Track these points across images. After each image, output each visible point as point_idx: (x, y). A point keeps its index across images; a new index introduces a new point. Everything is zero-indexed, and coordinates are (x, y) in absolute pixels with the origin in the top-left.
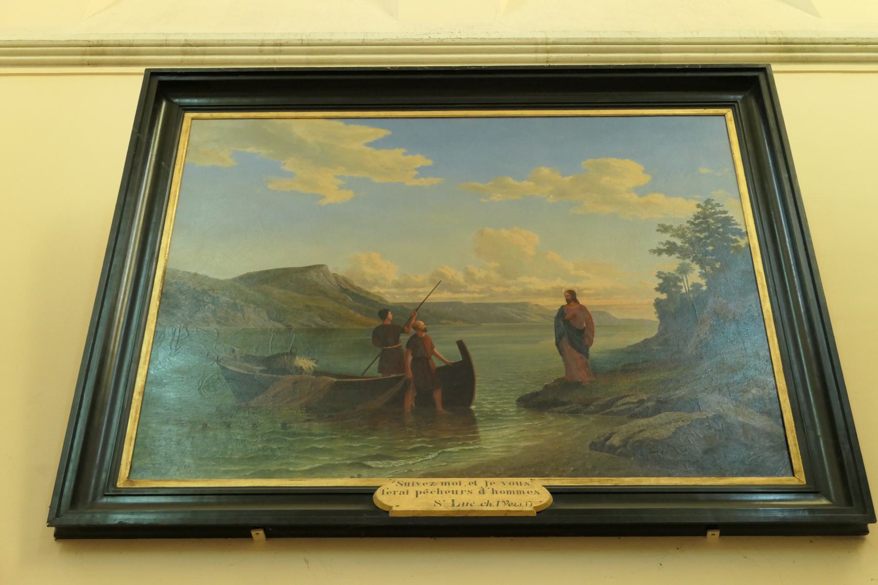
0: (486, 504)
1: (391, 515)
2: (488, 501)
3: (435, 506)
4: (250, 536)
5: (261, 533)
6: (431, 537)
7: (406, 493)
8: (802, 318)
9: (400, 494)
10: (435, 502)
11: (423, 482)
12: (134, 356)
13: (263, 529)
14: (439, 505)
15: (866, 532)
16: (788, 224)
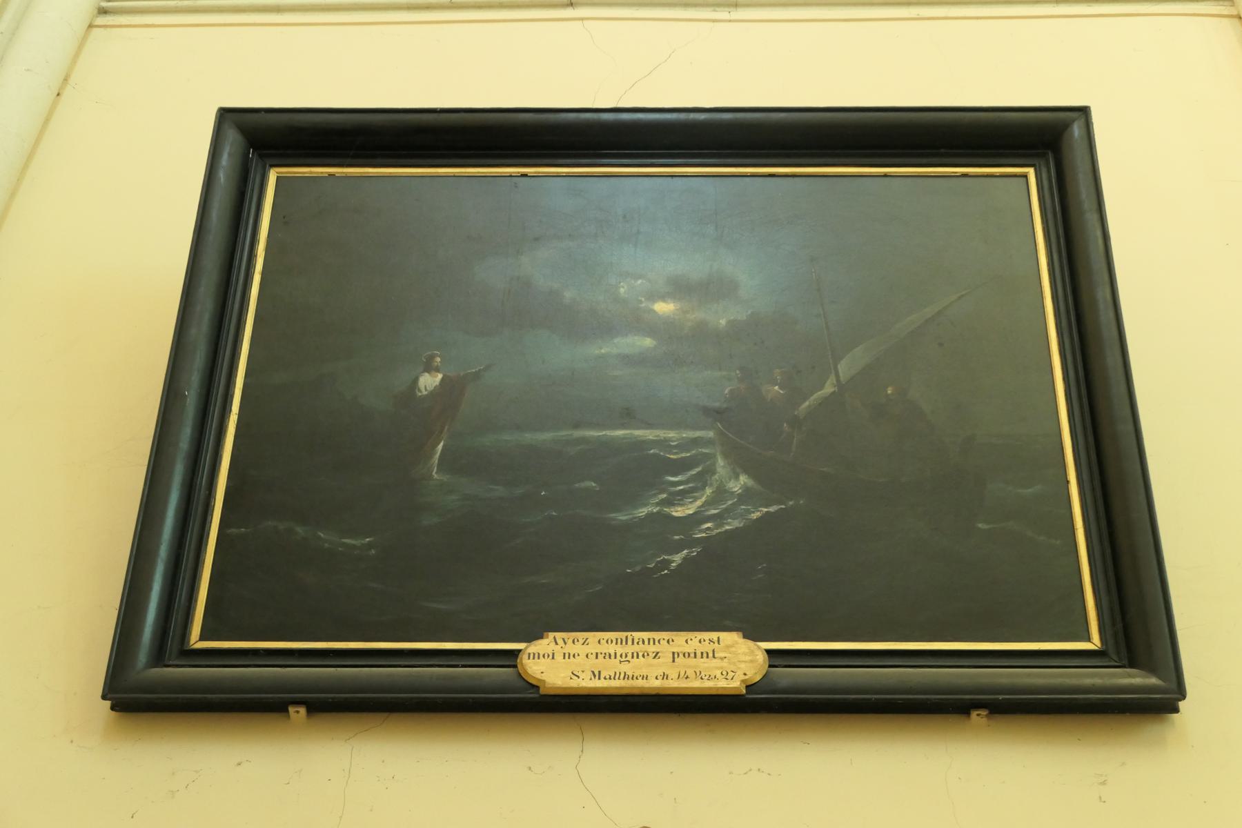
0: (662, 677)
1: (542, 691)
2: (664, 673)
3: (571, 678)
4: (287, 711)
5: (303, 710)
6: (675, 713)
7: (613, 657)
8: (672, 476)
9: (604, 657)
10: (573, 673)
11: (666, 638)
12: (1226, 13)
13: (304, 706)
14: (577, 678)
15: (1176, 710)
16: (230, 275)
